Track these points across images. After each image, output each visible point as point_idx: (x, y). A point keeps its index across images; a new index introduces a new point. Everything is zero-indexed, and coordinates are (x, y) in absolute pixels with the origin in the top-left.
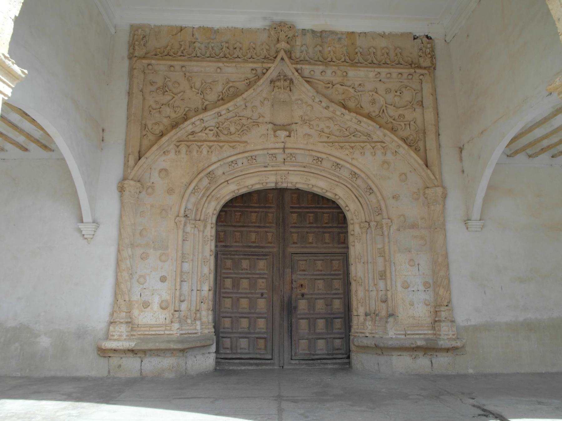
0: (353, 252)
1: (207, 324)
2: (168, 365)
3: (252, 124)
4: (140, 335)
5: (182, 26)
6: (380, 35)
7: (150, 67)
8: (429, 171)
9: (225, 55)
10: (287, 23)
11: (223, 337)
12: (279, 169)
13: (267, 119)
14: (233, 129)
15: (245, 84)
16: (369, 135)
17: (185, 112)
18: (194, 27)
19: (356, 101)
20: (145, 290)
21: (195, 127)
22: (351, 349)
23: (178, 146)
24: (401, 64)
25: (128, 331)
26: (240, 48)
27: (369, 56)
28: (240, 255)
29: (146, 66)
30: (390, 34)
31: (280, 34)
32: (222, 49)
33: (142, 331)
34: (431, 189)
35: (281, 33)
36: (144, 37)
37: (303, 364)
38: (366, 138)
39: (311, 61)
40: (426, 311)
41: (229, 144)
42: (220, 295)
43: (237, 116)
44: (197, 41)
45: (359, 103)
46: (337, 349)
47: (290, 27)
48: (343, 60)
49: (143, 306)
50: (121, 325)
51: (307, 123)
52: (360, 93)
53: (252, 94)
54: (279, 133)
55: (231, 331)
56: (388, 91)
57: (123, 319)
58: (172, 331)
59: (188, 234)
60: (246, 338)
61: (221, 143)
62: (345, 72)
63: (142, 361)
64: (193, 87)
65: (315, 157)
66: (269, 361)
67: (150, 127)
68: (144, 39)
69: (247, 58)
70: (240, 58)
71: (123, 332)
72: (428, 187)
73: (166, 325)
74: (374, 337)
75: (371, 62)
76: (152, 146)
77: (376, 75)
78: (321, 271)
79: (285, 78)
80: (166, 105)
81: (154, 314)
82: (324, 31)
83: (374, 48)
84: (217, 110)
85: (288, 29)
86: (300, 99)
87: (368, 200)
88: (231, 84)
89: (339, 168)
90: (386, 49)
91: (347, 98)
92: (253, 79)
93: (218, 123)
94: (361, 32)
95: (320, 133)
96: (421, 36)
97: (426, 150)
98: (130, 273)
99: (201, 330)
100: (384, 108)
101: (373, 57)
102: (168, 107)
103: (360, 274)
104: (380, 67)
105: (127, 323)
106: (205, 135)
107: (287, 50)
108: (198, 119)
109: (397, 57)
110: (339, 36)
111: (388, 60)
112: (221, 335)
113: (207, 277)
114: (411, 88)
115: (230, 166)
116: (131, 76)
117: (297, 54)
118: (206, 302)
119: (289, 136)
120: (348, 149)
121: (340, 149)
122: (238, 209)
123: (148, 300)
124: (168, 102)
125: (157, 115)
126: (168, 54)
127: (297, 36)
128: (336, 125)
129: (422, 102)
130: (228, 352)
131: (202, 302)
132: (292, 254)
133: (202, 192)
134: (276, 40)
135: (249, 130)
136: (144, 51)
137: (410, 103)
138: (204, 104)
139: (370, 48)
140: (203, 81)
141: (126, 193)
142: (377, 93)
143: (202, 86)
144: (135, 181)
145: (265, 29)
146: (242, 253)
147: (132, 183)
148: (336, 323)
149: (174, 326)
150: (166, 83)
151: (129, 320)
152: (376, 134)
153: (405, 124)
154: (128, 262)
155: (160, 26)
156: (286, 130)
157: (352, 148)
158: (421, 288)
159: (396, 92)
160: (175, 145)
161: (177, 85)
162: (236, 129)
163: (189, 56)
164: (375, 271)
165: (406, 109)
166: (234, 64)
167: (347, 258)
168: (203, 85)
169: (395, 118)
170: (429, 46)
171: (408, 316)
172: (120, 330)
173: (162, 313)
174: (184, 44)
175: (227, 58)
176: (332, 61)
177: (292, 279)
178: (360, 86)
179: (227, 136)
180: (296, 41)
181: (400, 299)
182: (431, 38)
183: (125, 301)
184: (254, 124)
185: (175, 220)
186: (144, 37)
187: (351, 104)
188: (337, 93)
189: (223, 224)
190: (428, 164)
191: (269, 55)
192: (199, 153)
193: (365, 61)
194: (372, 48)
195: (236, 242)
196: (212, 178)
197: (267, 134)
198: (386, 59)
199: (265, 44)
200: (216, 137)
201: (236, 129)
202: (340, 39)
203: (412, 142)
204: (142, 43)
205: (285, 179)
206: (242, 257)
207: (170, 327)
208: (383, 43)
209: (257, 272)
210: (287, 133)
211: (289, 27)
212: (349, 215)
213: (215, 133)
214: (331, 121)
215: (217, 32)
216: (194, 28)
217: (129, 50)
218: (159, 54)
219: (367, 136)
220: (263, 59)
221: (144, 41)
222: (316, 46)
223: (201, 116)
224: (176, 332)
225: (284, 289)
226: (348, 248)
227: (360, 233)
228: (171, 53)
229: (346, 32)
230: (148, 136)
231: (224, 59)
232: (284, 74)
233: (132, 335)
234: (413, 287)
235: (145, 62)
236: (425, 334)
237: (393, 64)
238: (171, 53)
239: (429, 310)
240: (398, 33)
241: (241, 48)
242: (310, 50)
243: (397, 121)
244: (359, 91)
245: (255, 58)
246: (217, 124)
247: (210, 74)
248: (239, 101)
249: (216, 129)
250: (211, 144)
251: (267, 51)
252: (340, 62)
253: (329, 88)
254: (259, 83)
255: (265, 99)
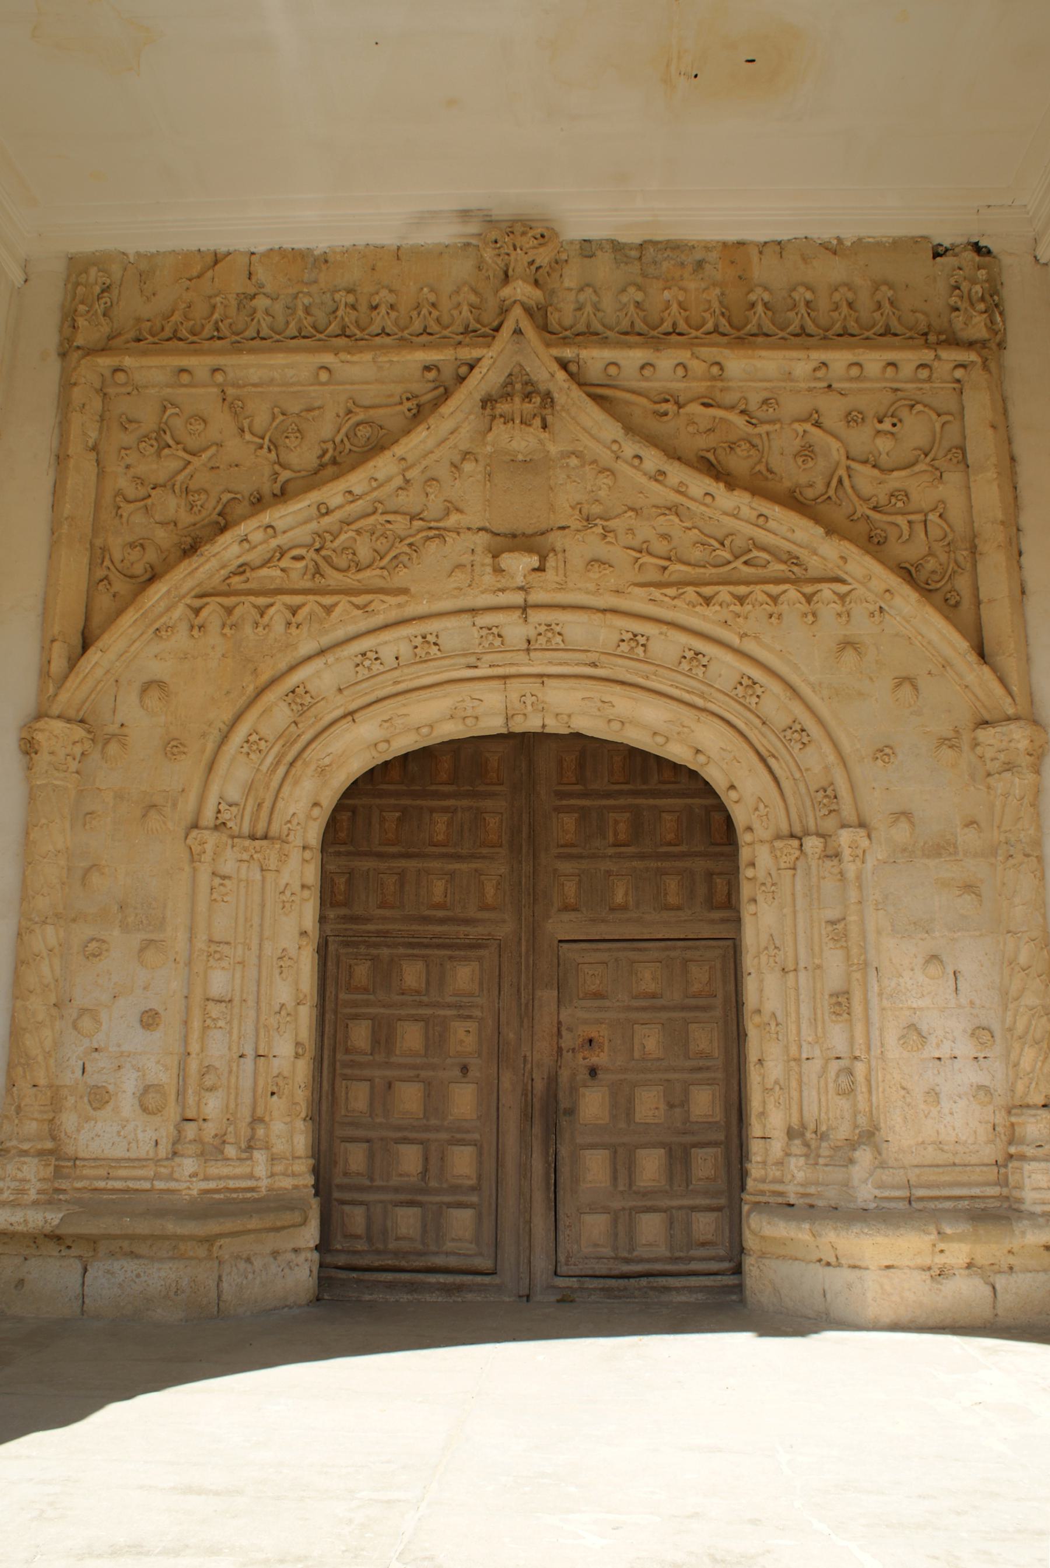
0: (752, 936)
1: (288, 1160)
2: (163, 1283)
3: (424, 534)
4: (79, 1189)
5: (218, 251)
6: (827, 249)
7: (121, 377)
8: (986, 669)
9: (344, 328)
10: (533, 224)
11: (343, 1202)
12: (512, 670)
13: (474, 517)
14: (364, 553)
15: (404, 413)
16: (793, 560)
17: (219, 508)
18: (253, 250)
19: (751, 453)
20: (96, 1055)
21: (248, 551)
22: (745, 1244)
23: (197, 611)
24: (896, 335)
25: (44, 1179)
26: (391, 305)
27: (794, 313)
28: (396, 945)
29: (107, 373)
30: (859, 242)
31: (512, 258)
32: (334, 312)
33: (86, 1178)
34: (994, 727)
35: (513, 253)
36: (106, 289)
37: (594, 1289)
38: (783, 567)
39: (609, 333)
40: (980, 1122)
41: (353, 599)
42: (335, 1070)
43: (380, 511)
44: (262, 290)
45: (764, 460)
46: (703, 1244)
47: (543, 236)
48: (709, 326)
49: (89, 1101)
50: (22, 1159)
51: (596, 525)
52: (767, 427)
53: (423, 442)
54: (508, 560)
55: (368, 1183)
56: (853, 418)
57: (29, 1140)
58: (177, 1180)
59: (227, 882)
60: (411, 1204)
61: (327, 596)
62: (718, 363)
63: (85, 1270)
64: (246, 429)
65: (624, 632)
66: (487, 1280)
67: (117, 556)
68: (106, 294)
69: (411, 335)
70: (388, 335)
71: (29, 1181)
72: (987, 723)
73: (157, 1162)
74: (812, 1206)
75: (800, 331)
76: (120, 612)
77: (815, 370)
78: (654, 996)
79: (529, 388)
80: (164, 486)
81: (124, 1127)
82: (651, 242)
83: (809, 288)
84: (314, 497)
85: (535, 241)
86: (573, 453)
87: (798, 766)
88: (361, 417)
89: (704, 666)
90: (846, 289)
91: (724, 445)
92: (429, 396)
93: (319, 536)
94: (767, 239)
95: (638, 555)
96: (958, 246)
97: (978, 603)
98: (53, 1000)
99: (269, 1180)
100: (842, 472)
101: (806, 315)
102: (171, 491)
103: (772, 1003)
104: (826, 348)
105: (41, 1153)
106: (279, 572)
107: (532, 303)
108: (259, 527)
109: (882, 314)
110: (698, 255)
111: (853, 323)
112: (336, 1195)
113: (288, 1014)
114: (926, 410)
115: (357, 669)
116: (64, 405)
117: (564, 313)
118: (286, 1091)
119: (541, 569)
120: (728, 605)
121: (701, 604)
122: (393, 801)
123: (104, 1084)
124: (173, 477)
125: (139, 518)
126: (175, 336)
127: (566, 261)
128: (690, 529)
129: (963, 449)
130: (359, 1247)
131: (273, 1094)
132: (560, 941)
133: (276, 749)
134: (502, 275)
135: (415, 554)
136: (106, 329)
137: (926, 455)
138: (278, 479)
139: (794, 289)
140: (276, 410)
141: (43, 759)
142: (820, 427)
143: (275, 424)
144: (69, 721)
145: (468, 244)
146: (402, 940)
147: (58, 726)
148: (700, 1161)
149: (179, 1165)
150: (166, 423)
151: (49, 1145)
152: (816, 555)
153: (909, 522)
154: (45, 969)
155: (152, 255)
156: (530, 550)
157: (741, 600)
158: (965, 1048)
159: (880, 422)
160: (188, 606)
161: (198, 427)
162: (375, 551)
163: (238, 338)
164: (818, 996)
165: (912, 475)
166: (368, 357)
167: (735, 952)
168: (278, 421)
169: (877, 503)
170: (982, 274)
171: (920, 1140)
172: (20, 1175)
173: (146, 1126)
174: (222, 303)
175: (348, 337)
176: (674, 332)
177: (559, 1023)
178: (765, 407)
179: (346, 574)
180: (561, 276)
181: (895, 1085)
182: (989, 252)
183: (34, 1086)
184: (432, 533)
185: (186, 838)
186: (106, 289)
187: (738, 463)
188: (691, 429)
189: (343, 849)
190: (986, 649)
191: (478, 321)
192: (260, 629)
193: (777, 328)
194: (801, 290)
195: (383, 905)
196: (301, 705)
197: (472, 566)
198: (845, 318)
199: (466, 289)
200: (314, 576)
201: (375, 551)
202: (700, 264)
203: (936, 578)
204: (99, 308)
205: (533, 703)
206: (401, 951)
207: (170, 1169)
208: (836, 271)
209: (449, 999)
210: (534, 561)
211: (539, 236)
212: (740, 816)
213: (311, 565)
214: (674, 518)
215: (324, 260)
216: (253, 254)
217: (61, 332)
218: (148, 336)
219: (789, 563)
220: (462, 334)
221: (104, 300)
222: (624, 290)
223: (266, 517)
224: (188, 1184)
225: (534, 1053)
226: (738, 921)
227: (774, 873)
228: (184, 331)
229: (718, 242)
230: (110, 584)
231: (342, 341)
232: (525, 378)
233: (57, 1191)
234: (938, 1046)
235: (105, 362)
236: (972, 1197)
237: (869, 334)
238: (184, 333)
239: (987, 1122)
240: (884, 240)
241: (392, 307)
242: (608, 303)
243: (885, 513)
244: (762, 422)
245: (437, 334)
246: (317, 539)
247: (299, 388)
248: (383, 466)
249: (312, 554)
250: (297, 600)
251: (471, 312)
252: (699, 333)
253: (666, 414)
254: (445, 409)
255: (466, 455)
